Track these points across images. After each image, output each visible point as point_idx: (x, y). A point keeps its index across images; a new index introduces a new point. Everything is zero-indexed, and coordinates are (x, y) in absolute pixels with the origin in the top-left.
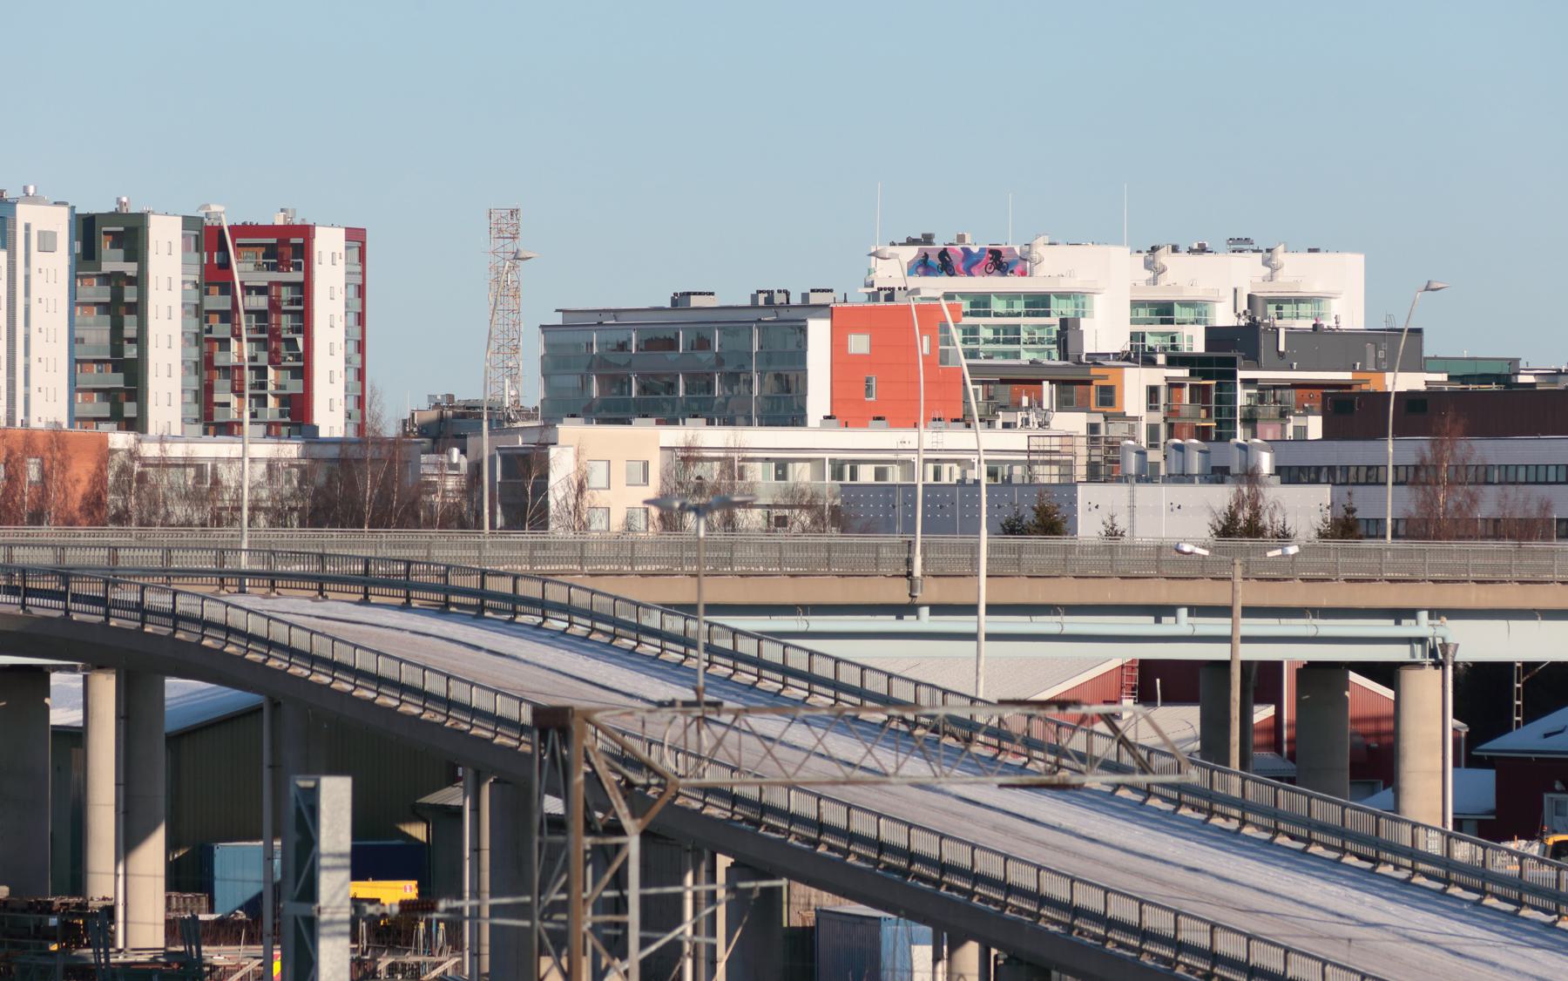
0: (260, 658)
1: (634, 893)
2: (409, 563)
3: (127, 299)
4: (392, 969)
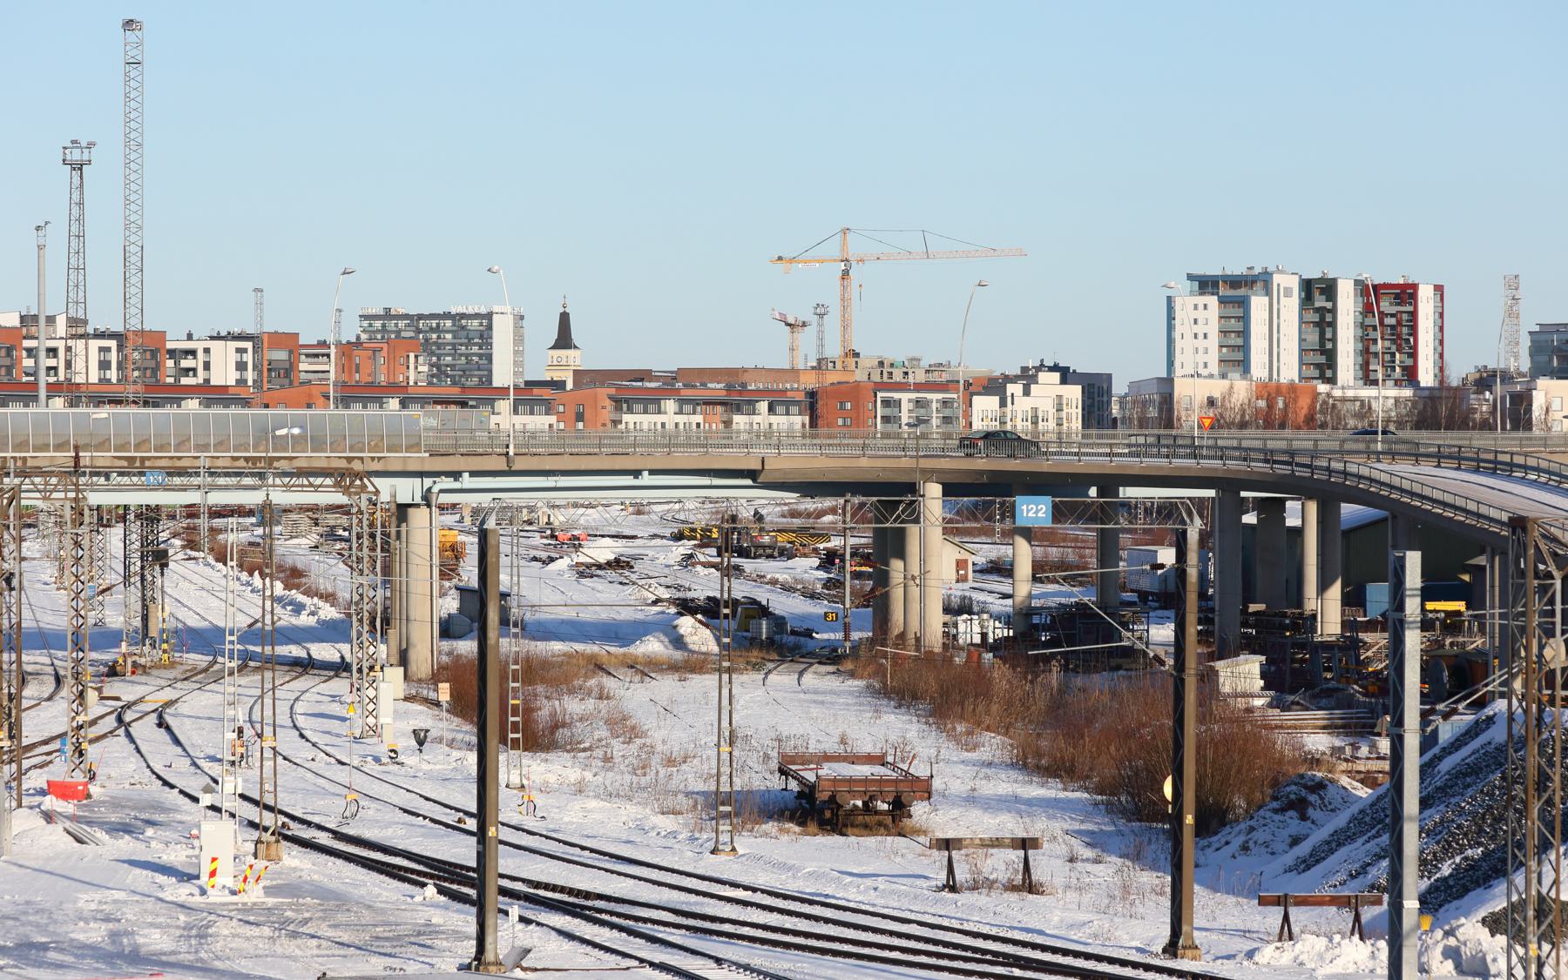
0: (1387, 493)
1: (1558, 607)
2: (1460, 447)
3: (1327, 320)
4: (1452, 644)
